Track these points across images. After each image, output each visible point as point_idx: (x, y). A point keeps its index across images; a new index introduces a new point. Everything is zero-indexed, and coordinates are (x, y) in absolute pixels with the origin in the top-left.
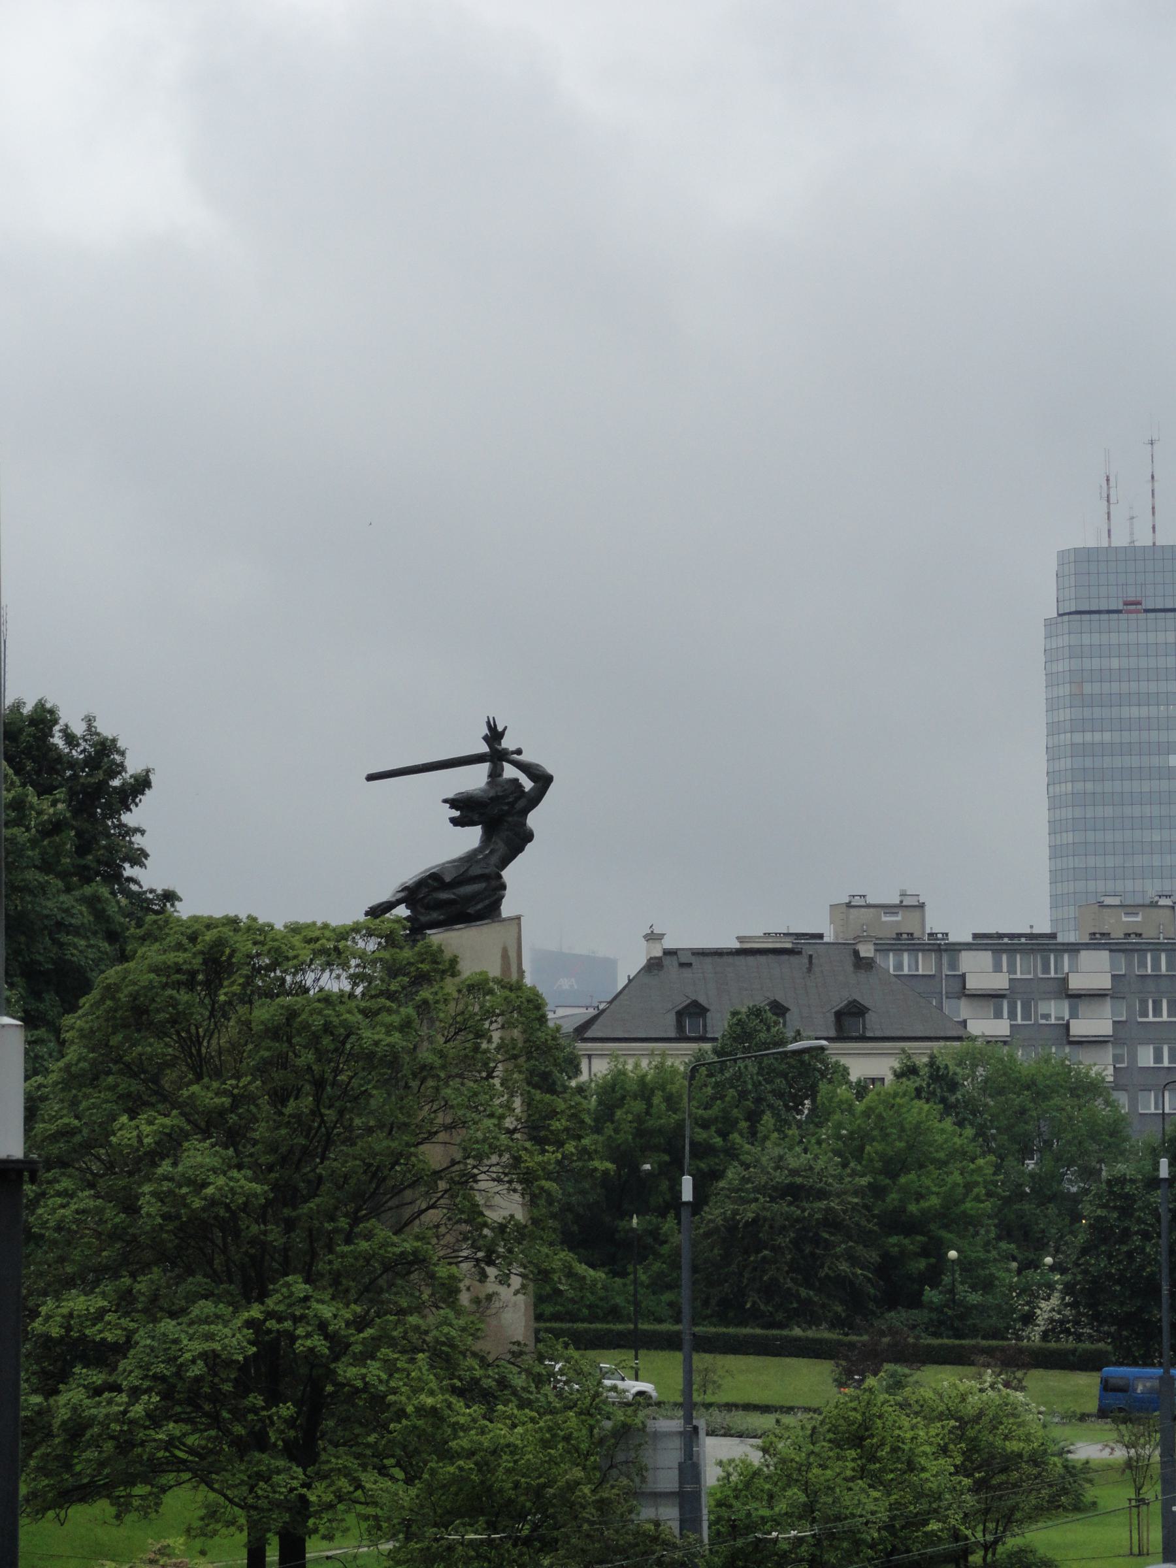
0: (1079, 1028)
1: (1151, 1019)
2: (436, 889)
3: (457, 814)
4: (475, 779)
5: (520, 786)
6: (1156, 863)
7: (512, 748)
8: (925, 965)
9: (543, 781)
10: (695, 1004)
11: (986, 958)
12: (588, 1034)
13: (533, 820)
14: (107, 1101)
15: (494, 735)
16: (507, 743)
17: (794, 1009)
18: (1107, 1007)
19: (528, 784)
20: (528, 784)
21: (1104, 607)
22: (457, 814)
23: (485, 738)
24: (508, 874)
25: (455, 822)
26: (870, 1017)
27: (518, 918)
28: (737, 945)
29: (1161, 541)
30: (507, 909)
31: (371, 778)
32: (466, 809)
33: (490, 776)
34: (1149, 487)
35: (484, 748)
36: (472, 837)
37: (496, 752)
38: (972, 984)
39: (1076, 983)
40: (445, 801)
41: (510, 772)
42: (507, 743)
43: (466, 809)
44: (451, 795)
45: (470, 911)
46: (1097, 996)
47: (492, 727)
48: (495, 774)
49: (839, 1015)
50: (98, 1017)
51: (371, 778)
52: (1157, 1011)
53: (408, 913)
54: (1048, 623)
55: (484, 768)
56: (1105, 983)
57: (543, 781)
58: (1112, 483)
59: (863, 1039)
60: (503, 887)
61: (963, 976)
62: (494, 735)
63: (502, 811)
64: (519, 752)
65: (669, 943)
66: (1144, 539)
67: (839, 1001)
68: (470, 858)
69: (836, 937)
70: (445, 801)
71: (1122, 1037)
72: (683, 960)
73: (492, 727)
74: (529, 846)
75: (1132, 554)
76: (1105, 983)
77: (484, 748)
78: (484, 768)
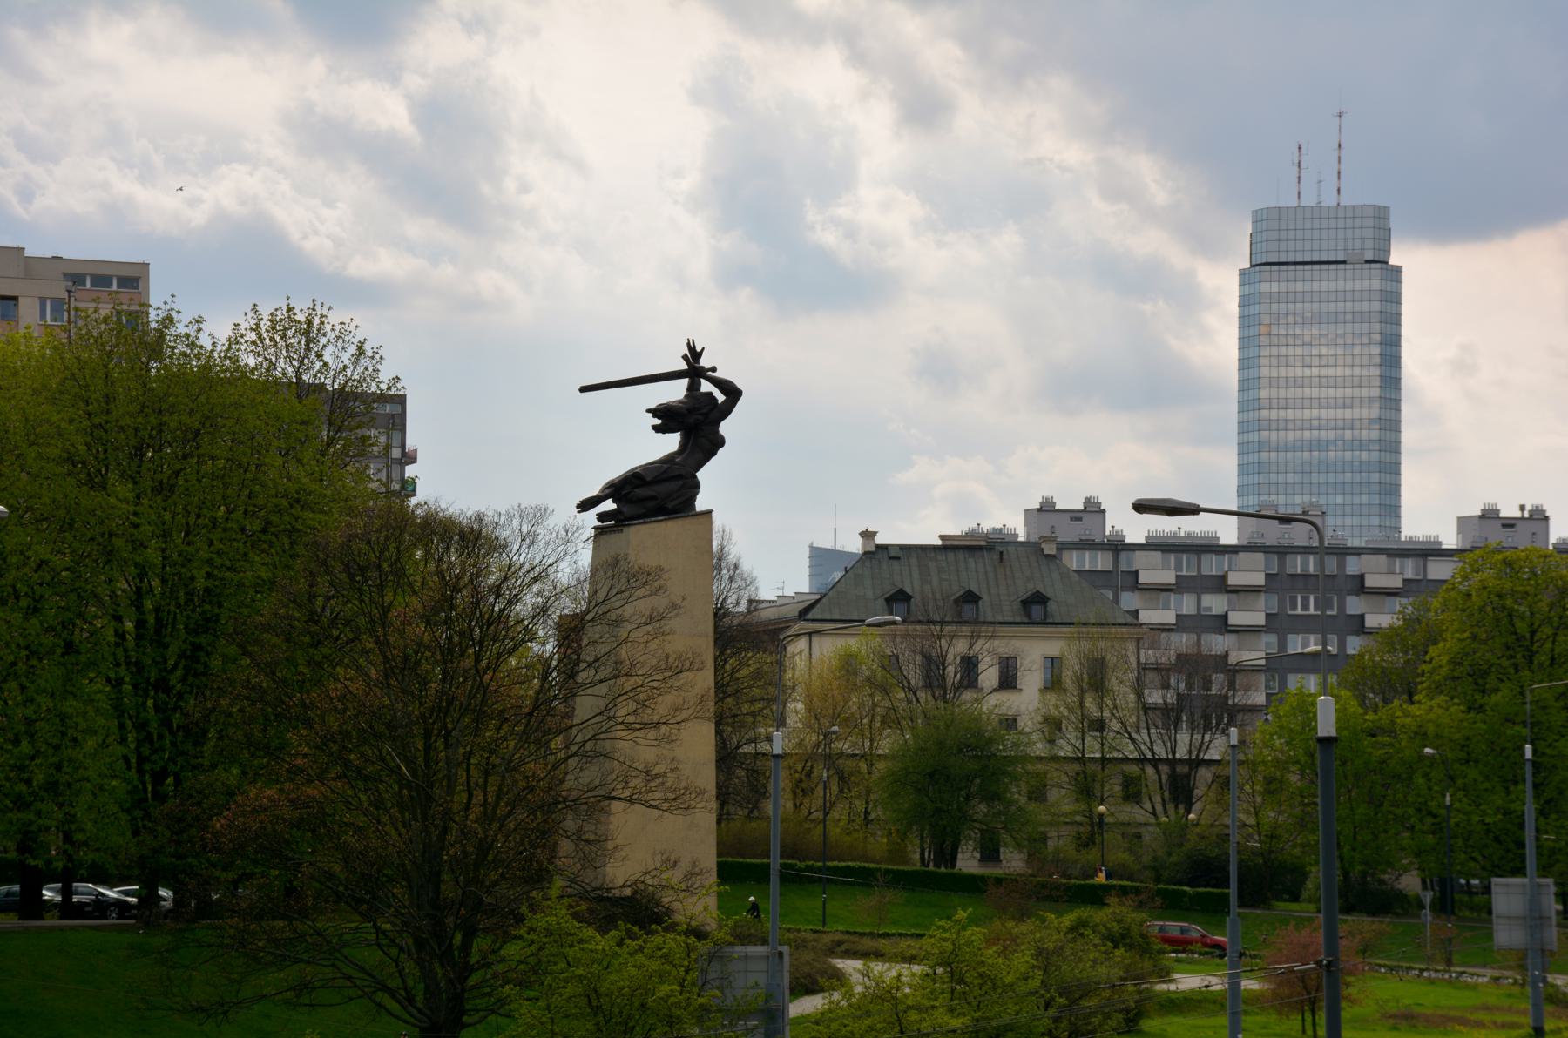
0: (1236, 619)
1: (1299, 611)
2: (637, 487)
3: (659, 422)
4: (676, 391)
5: (715, 399)
6: (1331, 475)
7: (708, 366)
8: (1102, 562)
9: (733, 393)
10: (901, 591)
11: (1157, 556)
12: (809, 616)
13: (725, 428)
14: (499, 729)
15: (694, 354)
16: (705, 362)
17: (985, 597)
18: (1262, 600)
19: (721, 398)
20: (721, 398)
21: (1308, 259)
22: (659, 422)
23: (685, 357)
24: (701, 475)
25: (656, 429)
26: (1052, 606)
27: (710, 512)
28: (939, 543)
29: (1346, 200)
30: (701, 504)
31: (583, 389)
32: (667, 418)
33: (689, 389)
34: (1336, 154)
35: (684, 366)
36: (671, 443)
37: (694, 369)
38: (1144, 578)
39: (1234, 579)
40: (649, 411)
41: (706, 386)
42: (705, 362)
43: (667, 418)
44: (653, 406)
45: (670, 506)
46: (1253, 590)
47: (692, 348)
48: (693, 388)
49: (1026, 604)
50: (754, 740)
51: (583, 389)
52: (1305, 607)
53: (614, 506)
54: (1243, 273)
55: (685, 382)
56: (1259, 579)
57: (733, 393)
58: (1304, 150)
59: (1044, 623)
60: (697, 486)
61: (1136, 572)
62: (694, 354)
63: (699, 417)
64: (714, 369)
65: (879, 540)
66: (1330, 199)
67: (1025, 590)
68: (669, 459)
69: (1028, 535)
70: (649, 411)
71: (1276, 624)
72: (893, 554)
73: (692, 348)
74: (721, 451)
75: (1318, 213)
76: (1259, 579)
77: (684, 366)
78: (685, 382)
